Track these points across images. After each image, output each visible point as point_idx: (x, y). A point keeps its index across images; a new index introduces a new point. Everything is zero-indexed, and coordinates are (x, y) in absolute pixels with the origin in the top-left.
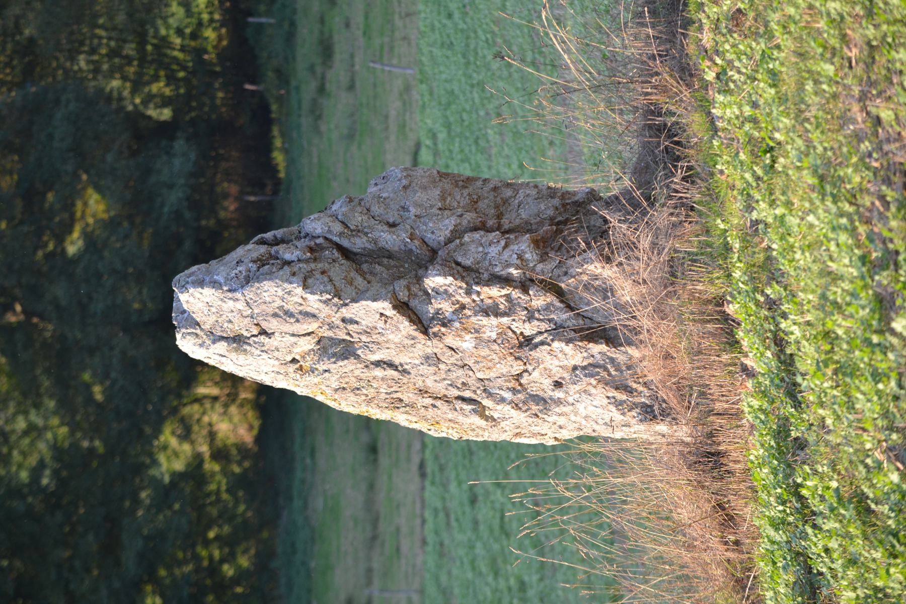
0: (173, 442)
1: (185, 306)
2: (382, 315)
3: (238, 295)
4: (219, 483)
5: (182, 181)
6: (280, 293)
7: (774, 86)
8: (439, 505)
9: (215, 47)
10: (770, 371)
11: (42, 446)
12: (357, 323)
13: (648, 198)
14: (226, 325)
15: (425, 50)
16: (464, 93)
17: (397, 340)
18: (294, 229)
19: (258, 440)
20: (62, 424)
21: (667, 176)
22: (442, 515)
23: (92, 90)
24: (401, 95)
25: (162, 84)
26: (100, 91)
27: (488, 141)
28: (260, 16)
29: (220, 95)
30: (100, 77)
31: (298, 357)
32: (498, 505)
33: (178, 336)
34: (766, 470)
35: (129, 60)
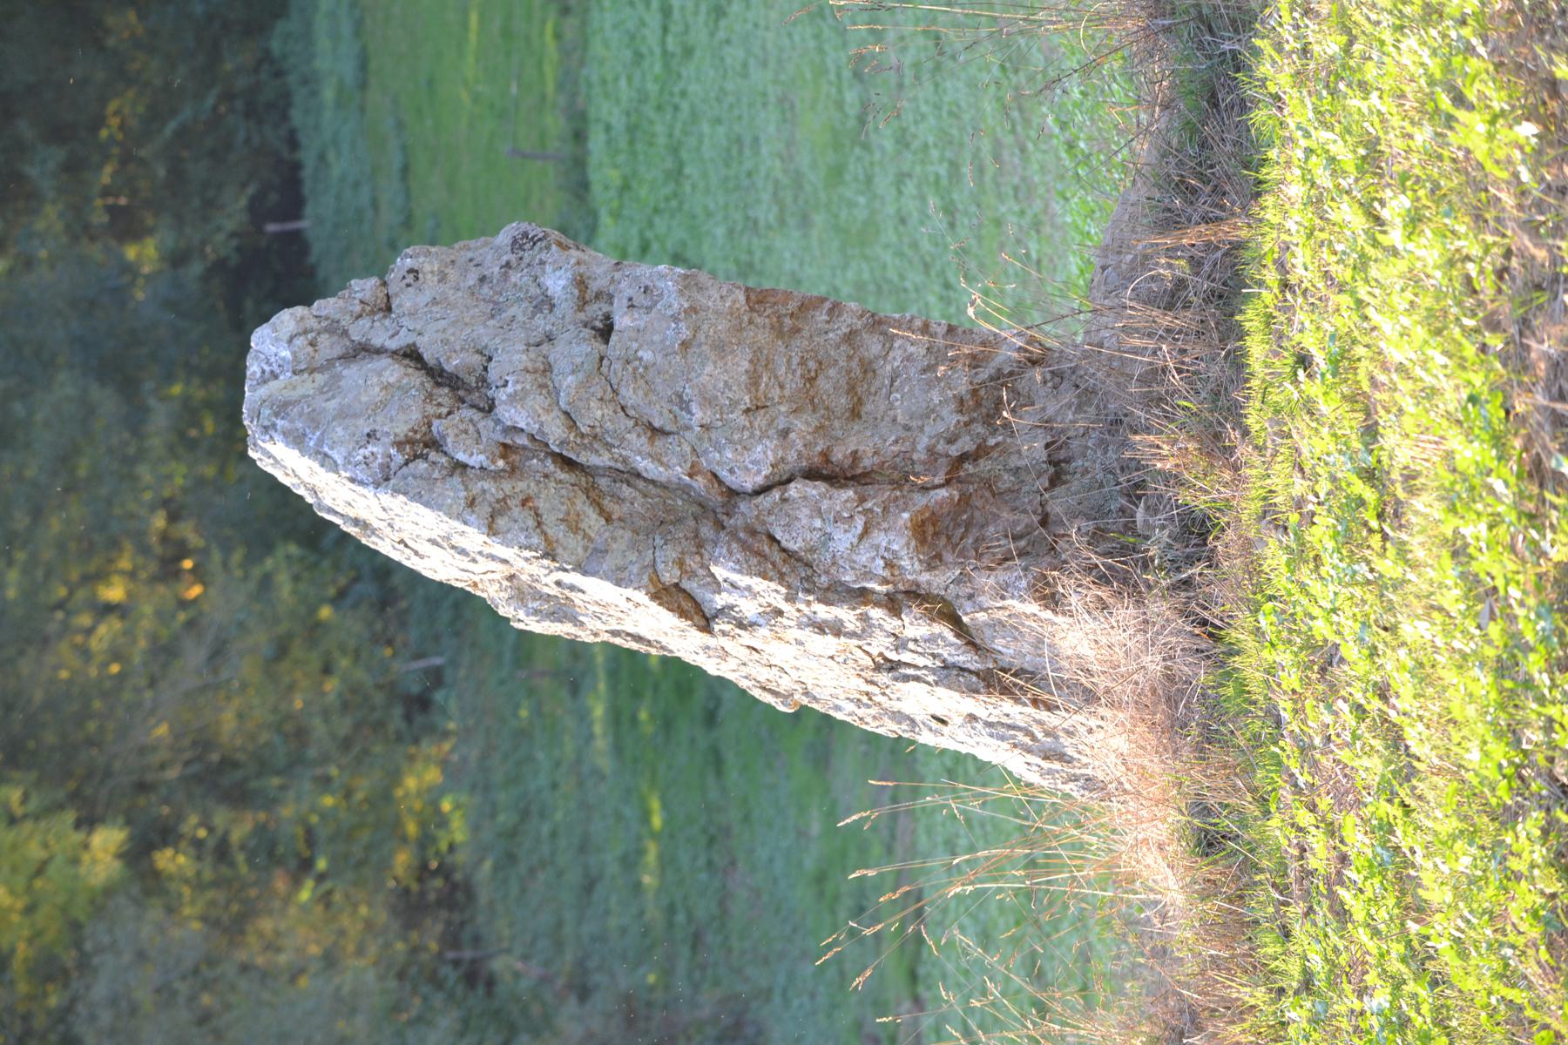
12: (584, 592)
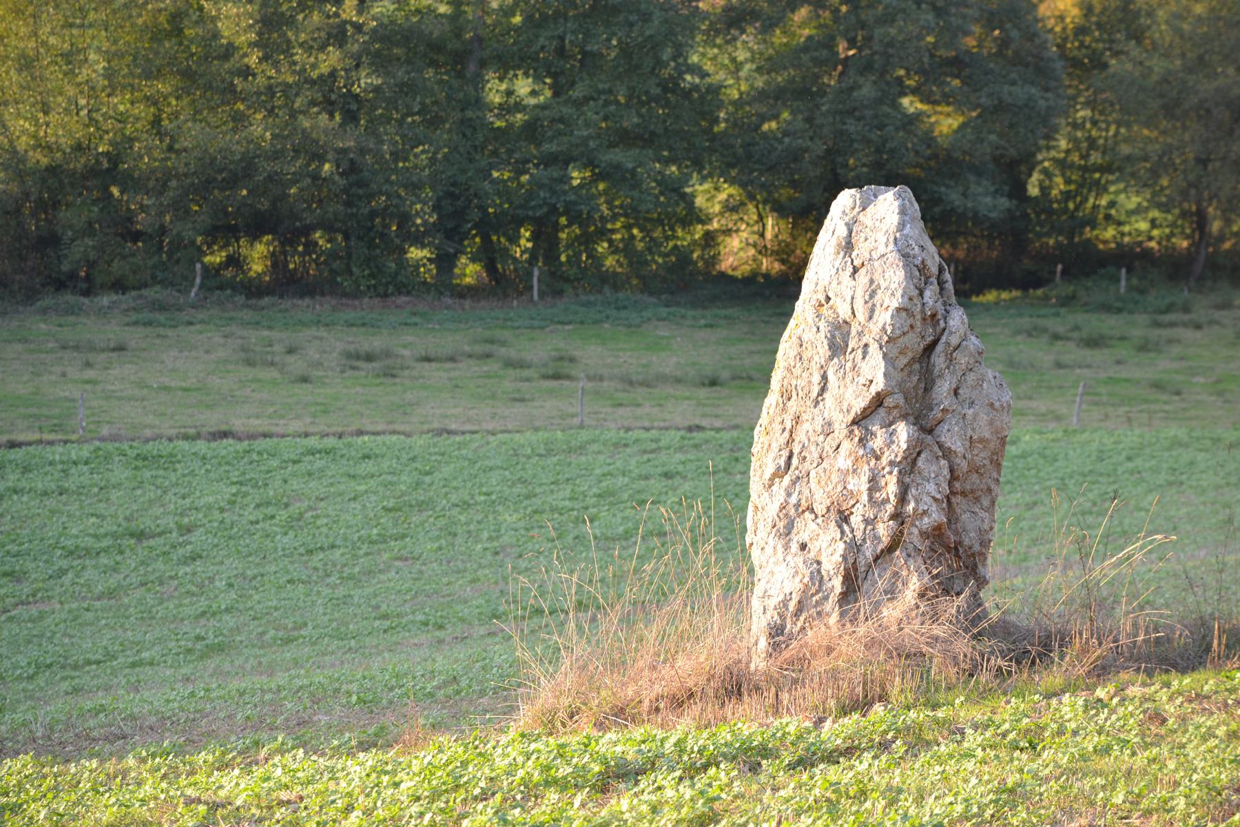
0: (722, 196)
1: (881, 197)
2: (871, 382)
3: (891, 246)
4: (684, 239)
5: (969, 205)
6: (893, 286)
7: (1095, 751)
8: (662, 444)
9: (1097, 237)
10: (822, 742)
11: (721, 75)
12: (864, 358)
13: (980, 634)
14: (863, 235)
15: (1096, 436)
16: (1055, 471)
17: (847, 396)
18: (953, 300)
19: (723, 275)
20: (741, 94)
21: (1001, 652)
22: (654, 446)
23: (1057, 121)
24: (1052, 412)
25: (1062, 187)
26: (1056, 129)
27: (1009, 493)
28: (1128, 279)
29: (1051, 242)
30: (1069, 129)
31: (831, 302)
32: (663, 498)
33: (853, 191)
34: (729, 737)
35: (1085, 157)
